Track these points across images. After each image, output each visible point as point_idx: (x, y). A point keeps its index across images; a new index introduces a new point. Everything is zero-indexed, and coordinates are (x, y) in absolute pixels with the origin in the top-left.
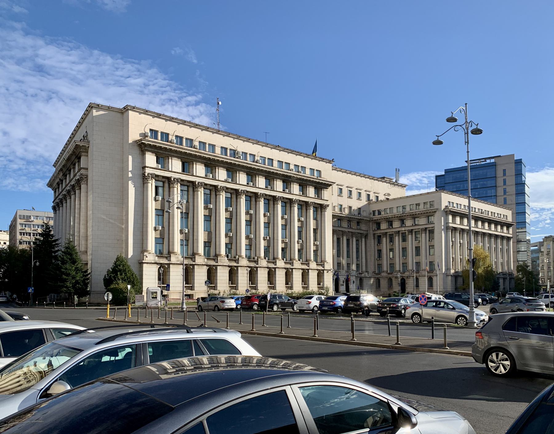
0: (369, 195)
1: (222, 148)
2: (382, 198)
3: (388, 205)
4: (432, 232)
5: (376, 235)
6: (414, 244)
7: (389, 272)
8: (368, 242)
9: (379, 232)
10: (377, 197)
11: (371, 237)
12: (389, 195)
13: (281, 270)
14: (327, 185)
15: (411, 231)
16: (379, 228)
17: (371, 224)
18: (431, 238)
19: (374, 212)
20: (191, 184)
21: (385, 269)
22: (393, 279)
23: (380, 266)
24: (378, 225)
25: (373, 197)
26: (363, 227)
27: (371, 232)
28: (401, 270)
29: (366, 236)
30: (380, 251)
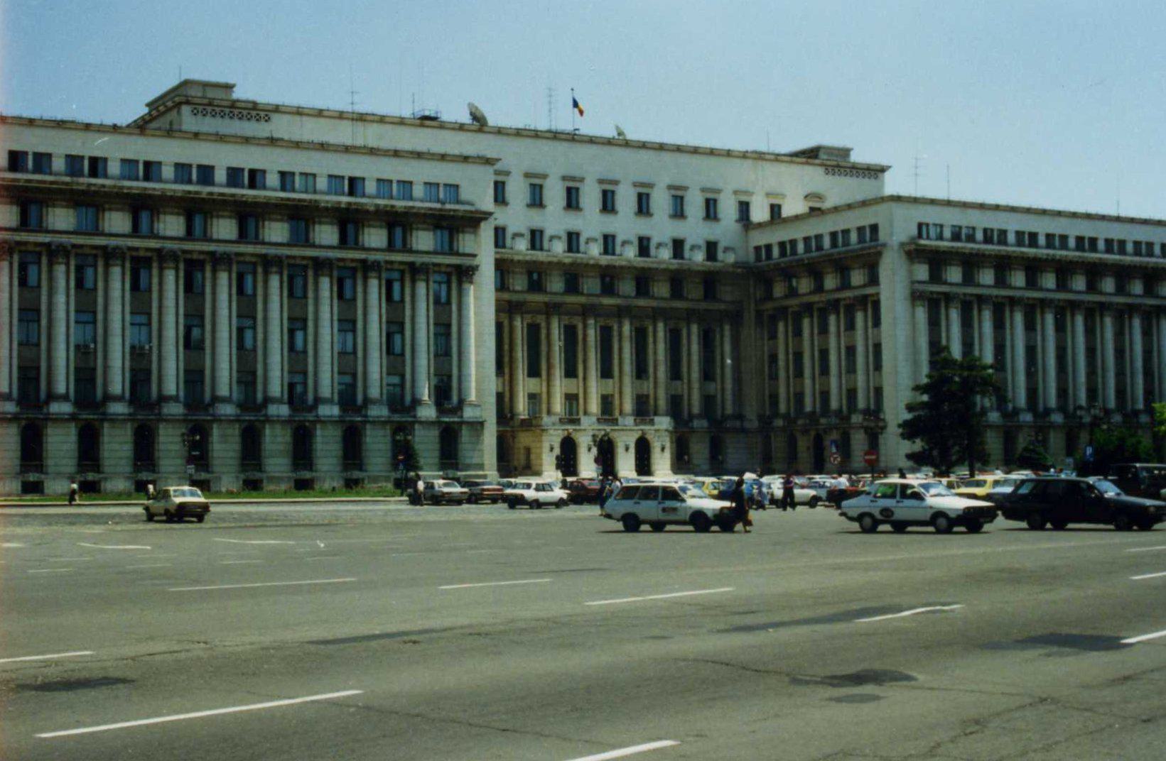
0: (744, 208)
1: (123, 161)
9: (769, 305)
10: (775, 210)
11: (749, 317)
14: (473, 220)
16: (769, 296)
17: (752, 282)
18: (877, 322)
19: (758, 249)
21: (782, 407)
22: (798, 435)
23: (774, 398)
24: (769, 285)
25: (759, 213)
27: (753, 305)
28: (845, 408)
30: (773, 358)
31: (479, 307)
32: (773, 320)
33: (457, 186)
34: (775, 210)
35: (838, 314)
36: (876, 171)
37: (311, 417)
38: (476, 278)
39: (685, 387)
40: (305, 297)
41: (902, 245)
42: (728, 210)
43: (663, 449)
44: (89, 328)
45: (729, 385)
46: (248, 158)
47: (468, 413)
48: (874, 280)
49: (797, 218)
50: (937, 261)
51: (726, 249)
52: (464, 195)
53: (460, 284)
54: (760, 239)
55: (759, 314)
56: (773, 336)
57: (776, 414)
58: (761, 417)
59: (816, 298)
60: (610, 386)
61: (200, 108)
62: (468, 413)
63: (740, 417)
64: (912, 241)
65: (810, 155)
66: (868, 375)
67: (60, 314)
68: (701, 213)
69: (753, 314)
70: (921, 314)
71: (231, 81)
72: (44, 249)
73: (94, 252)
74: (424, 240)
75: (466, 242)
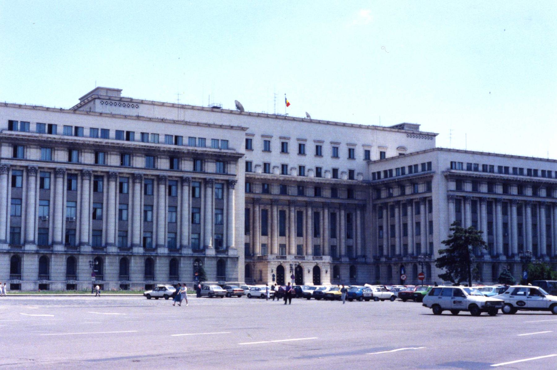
0: (367, 154)
2: (391, 153)
3: (406, 163)
4: (430, 202)
5: (377, 206)
6: (389, 222)
7: (390, 256)
9: (379, 202)
10: (382, 154)
11: (370, 207)
12: (403, 148)
13: (163, 258)
15: (410, 202)
16: (379, 197)
18: (431, 211)
20: (52, 171)
21: (385, 252)
22: (392, 265)
23: (381, 247)
24: (402, 188)
25: (375, 156)
27: (371, 201)
29: (363, 208)
31: (237, 199)
32: (381, 209)
33: (228, 141)
34: (382, 154)
35: (412, 206)
36: (431, 136)
37: (154, 254)
38: (236, 186)
39: (338, 241)
40: (153, 194)
41: (443, 172)
43: (326, 272)
44: (46, 208)
45: (359, 241)
46: (197, 133)
47: (231, 253)
48: (429, 189)
49: (393, 158)
50: (460, 180)
51: (359, 174)
52: (230, 146)
53: (228, 189)
54: (375, 169)
55: (374, 206)
56: (381, 217)
57: (382, 255)
58: (375, 257)
59: (400, 198)
60: (283, 240)
61: (105, 101)
62: (231, 253)
63: (364, 256)
64: (448, 170)
65: (400, 128)
66: (426, 236)
67: (32, 201)
68: (347, 155)
69: (371, 207)
70: (452, 206)
71: (120, 88)
73: (49, 171)
74: (211, 167)
75: (231, 169)
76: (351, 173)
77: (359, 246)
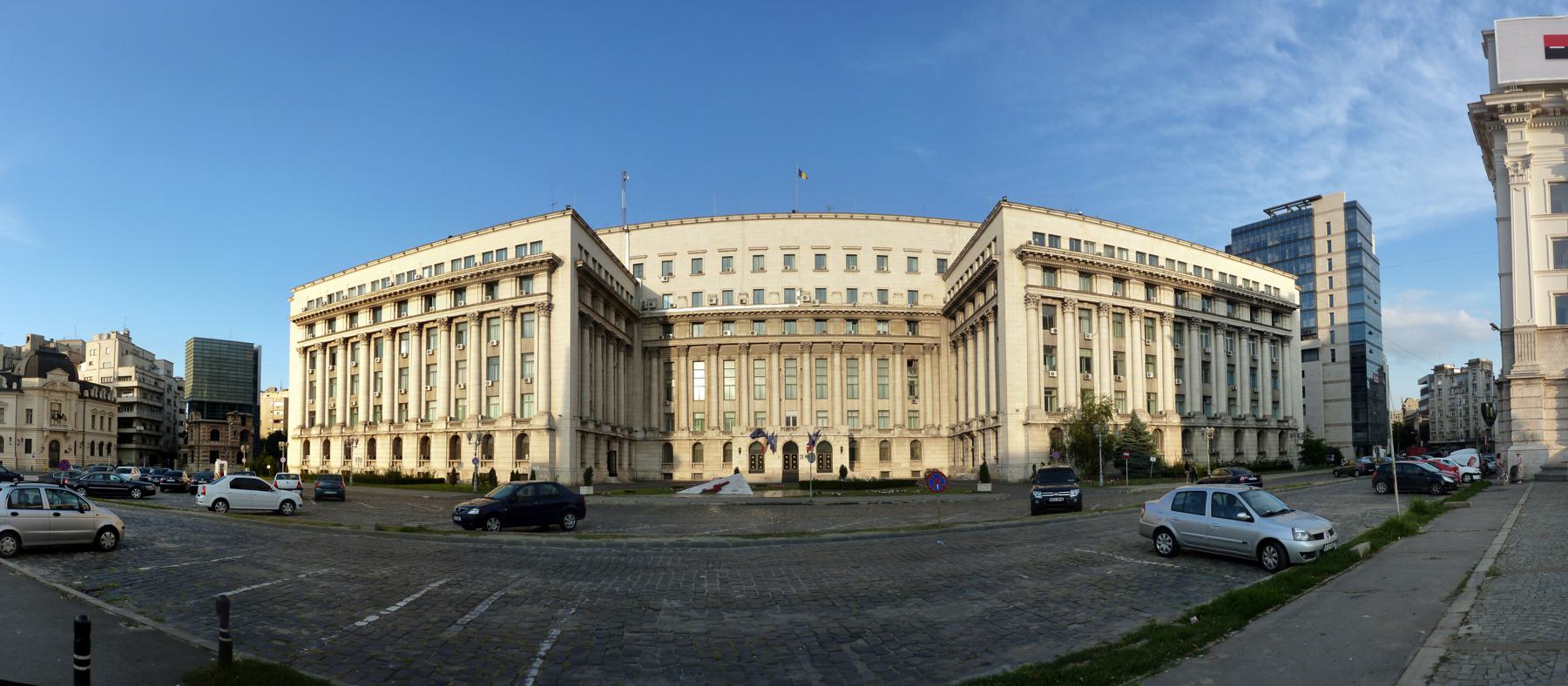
8: (943, 359)
26: (928, 330)
42: (928, 265)
45: (929, 402)
70: (1035, 318)
72: (1058, 303)
76: (852, 292)
77: (929, 411)
